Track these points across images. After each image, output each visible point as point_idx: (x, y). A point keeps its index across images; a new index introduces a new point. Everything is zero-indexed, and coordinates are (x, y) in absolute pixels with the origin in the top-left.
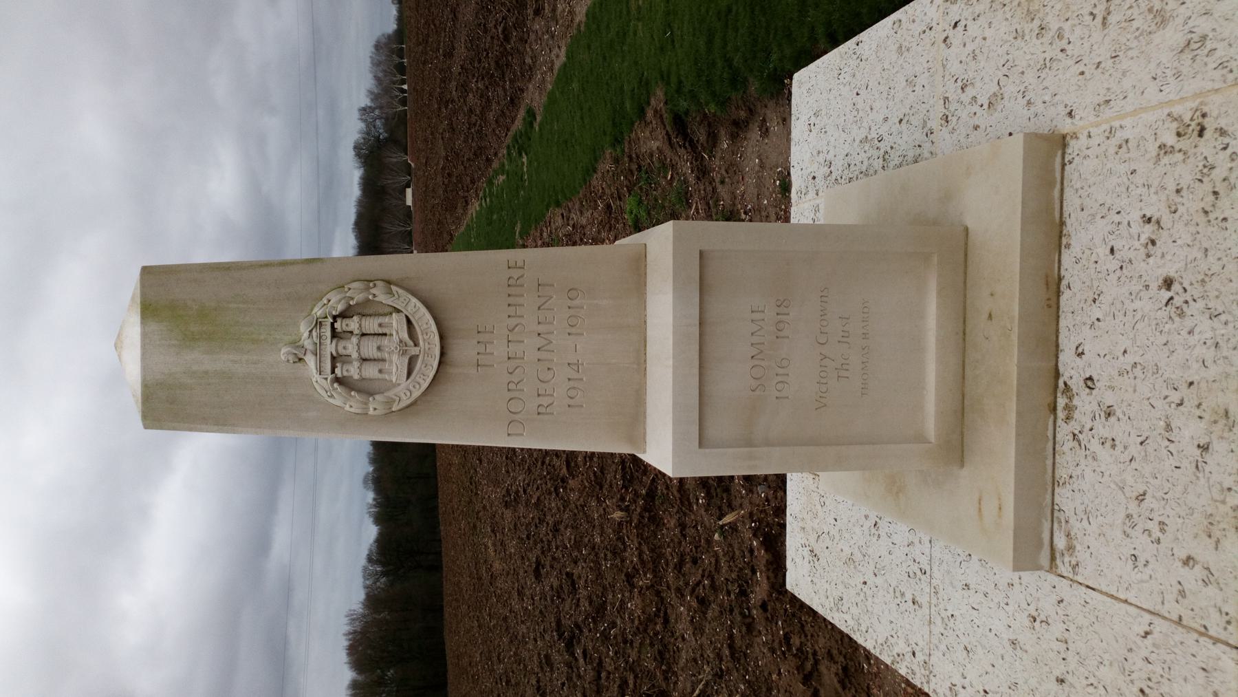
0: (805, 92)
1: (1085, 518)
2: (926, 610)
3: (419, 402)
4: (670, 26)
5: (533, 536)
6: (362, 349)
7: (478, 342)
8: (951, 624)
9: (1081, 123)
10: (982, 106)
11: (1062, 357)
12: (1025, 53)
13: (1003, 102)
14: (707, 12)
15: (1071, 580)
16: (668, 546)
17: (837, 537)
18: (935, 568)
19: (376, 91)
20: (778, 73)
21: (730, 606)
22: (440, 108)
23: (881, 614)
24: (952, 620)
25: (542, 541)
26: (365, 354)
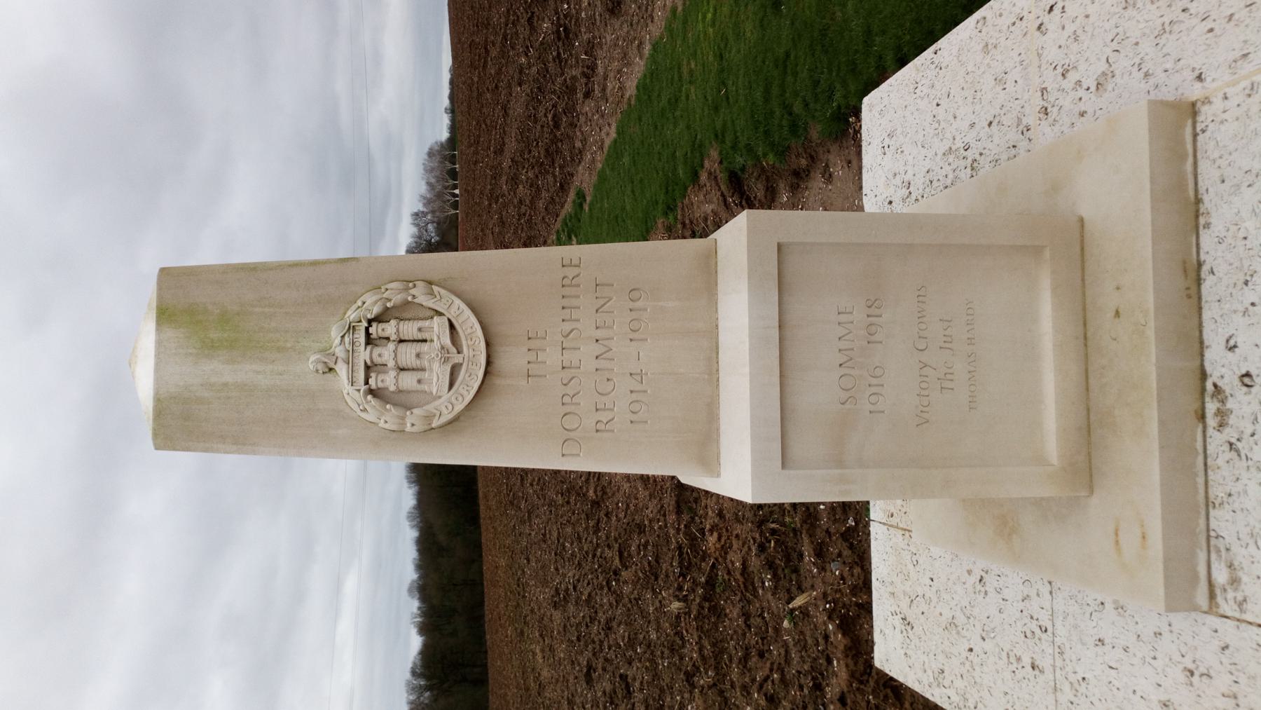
0: (877, 115)
1: (1251, 542)
2: (1049, 675)
3: (462, 418)
4: (724, 84)
5: (584, 636)
6: (399, 355)
7: (529, 350)
8: (1082, 689)
9: (1215, 85)
10: (1088, 89)
11: (1208, 355)
12: (1138, 21)
13: (1114, 79)
14: (764, 62)
15: (1238, 620)
16: (732, 639)
17: (935, 600)
18: (1058, 623)
19: (428, 196)
20: (842, 111)
21: (804, 702)
22: (490, 205)
23: (993, 685)
24: (1084, 685)
25: (594, 642)
26: (403, 363)
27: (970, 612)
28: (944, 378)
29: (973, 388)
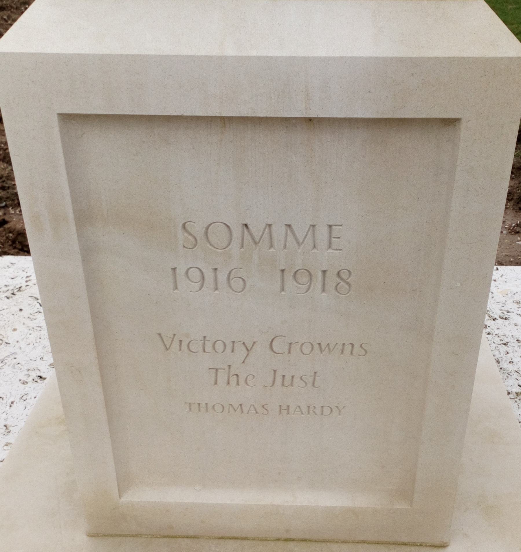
17: (31, 324)
21: (9, 188)
27: (8, 364)
28: (231, 374)
29: (218, 408)
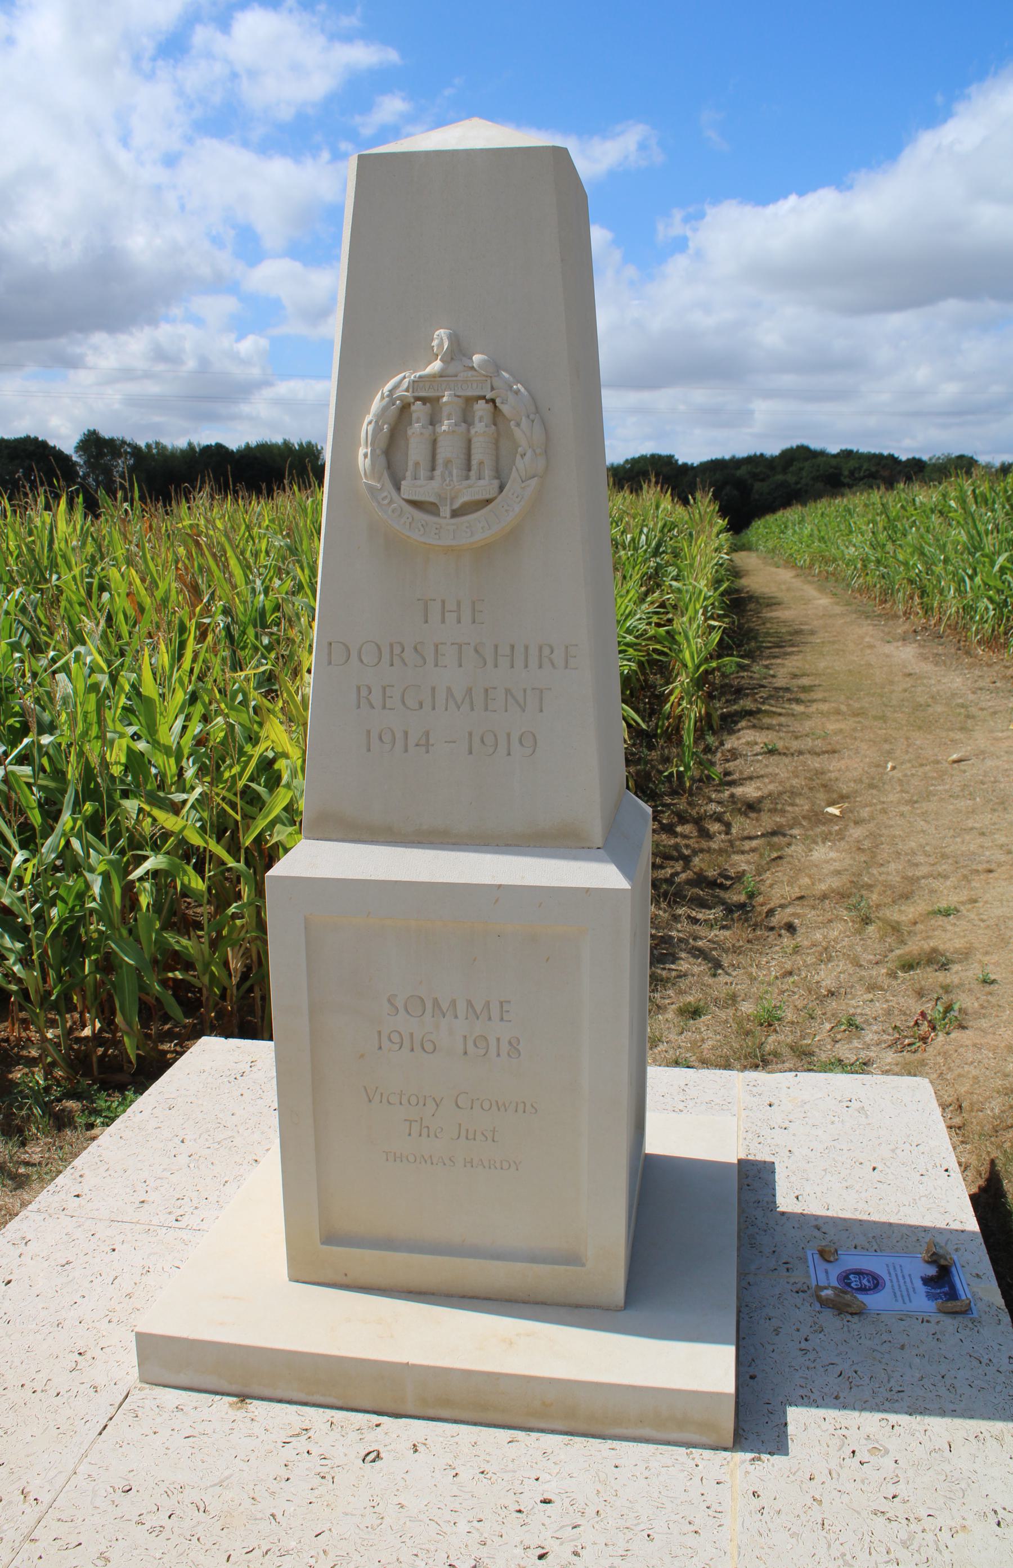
10: (806, 1340)
24: (108, 1249)
